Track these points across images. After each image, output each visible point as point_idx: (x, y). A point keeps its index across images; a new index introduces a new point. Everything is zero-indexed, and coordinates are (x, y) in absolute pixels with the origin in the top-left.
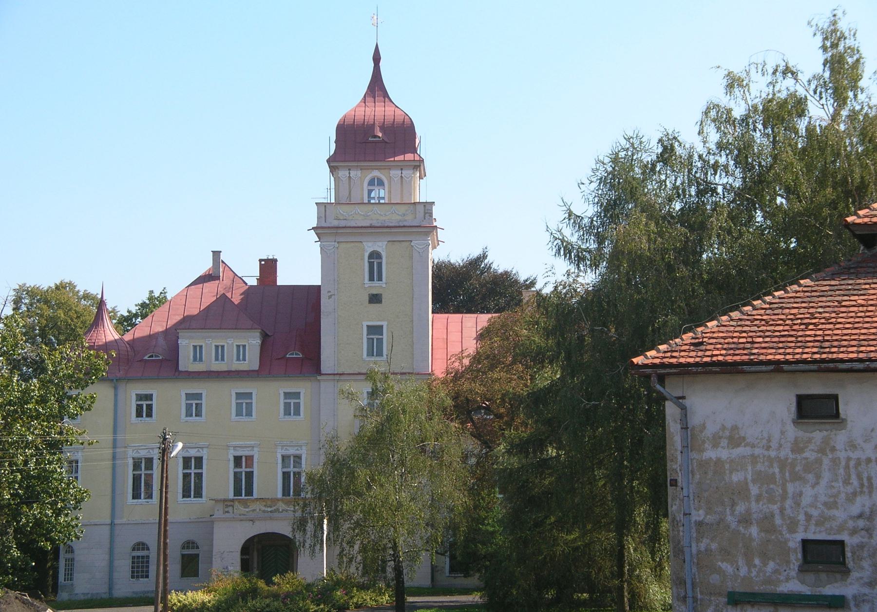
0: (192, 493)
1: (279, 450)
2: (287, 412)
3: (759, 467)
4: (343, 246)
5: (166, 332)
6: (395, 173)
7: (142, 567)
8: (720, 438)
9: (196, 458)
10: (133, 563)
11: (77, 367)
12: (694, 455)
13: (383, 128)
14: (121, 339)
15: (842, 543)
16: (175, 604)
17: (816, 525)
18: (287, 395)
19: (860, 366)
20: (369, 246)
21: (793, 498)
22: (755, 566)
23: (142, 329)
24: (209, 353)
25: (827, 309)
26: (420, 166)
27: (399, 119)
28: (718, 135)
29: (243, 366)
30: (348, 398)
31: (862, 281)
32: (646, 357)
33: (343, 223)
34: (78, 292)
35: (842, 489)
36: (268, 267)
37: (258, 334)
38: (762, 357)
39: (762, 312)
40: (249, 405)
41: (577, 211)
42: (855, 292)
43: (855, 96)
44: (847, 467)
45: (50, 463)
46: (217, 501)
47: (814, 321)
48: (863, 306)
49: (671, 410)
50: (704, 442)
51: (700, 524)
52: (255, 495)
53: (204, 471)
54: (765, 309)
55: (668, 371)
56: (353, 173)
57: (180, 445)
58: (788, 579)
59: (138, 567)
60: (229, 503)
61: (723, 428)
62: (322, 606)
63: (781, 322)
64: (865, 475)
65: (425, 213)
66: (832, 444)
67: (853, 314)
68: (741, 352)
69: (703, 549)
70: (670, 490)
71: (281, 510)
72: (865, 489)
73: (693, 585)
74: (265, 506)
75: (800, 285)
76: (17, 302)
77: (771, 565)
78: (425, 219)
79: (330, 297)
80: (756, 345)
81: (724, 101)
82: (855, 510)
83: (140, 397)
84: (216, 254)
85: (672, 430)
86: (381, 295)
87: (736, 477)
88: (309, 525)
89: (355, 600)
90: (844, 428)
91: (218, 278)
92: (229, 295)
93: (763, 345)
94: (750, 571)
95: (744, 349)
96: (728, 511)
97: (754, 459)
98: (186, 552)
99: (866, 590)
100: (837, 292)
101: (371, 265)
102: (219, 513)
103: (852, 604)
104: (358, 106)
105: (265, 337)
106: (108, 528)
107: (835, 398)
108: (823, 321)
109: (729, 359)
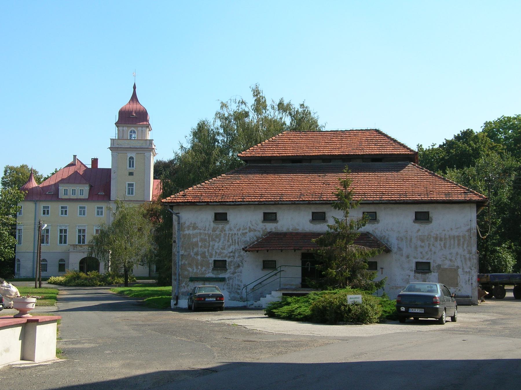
0: (82, 242)
1: (77, 227)
2: (98, 214)
3: (202, 236)
5: (55, 184)
6: (140, 129)
8: (190, 227)
9: (64, 230)
11: (14, 196)
12: (181, 232)
13: (136, 112)
14: (38, 186)
15: (226, 261)
16: (52, 281)
17: (218, 255)
18: (98, 208)
19: (233, 203)
20: (129, 155)
21: (212, 247)
22: (199, 269)
23: (46, 183)
24: (70, 192)
25: (228, 184)
26: (149, 126)
27: (142, 109)
28: (221, 123)
29: (82, 197)
30: (109, 210)
31: (241, 175)
32: (166, 199)
33: (120, 146)
34: (29, 168)
35: (227, 244)
36: (95, 161)
38: (203, 200)
39: (208, 185)
40: (84, 211)
41: (184, 146)
42: (237, 179)
43: (266, 112)
44: (229, 236)
45: (2, 230)
46: (71, 245)
47: (222, 188)
48: (239, 183)
49: (174, 217)
50: (185, 228)
51: (182, 255)
52: (86, 244)
53: (49, 234)
54: (209, 184)
55: (173, 204)
57: (46, 225)
58: (209, 273)
60: (75, 246)
61: (191, 224)
62: (102, 283)
63: (212, 188)
64: (234, 239)
65: (150, 143)
66: (225, 229)
67: (235, 186)
68: (198, 198)
69: (183, 263)
70: (173, 244)
72: (233, 244)
73: (179, 275)
75: (221, 176)
76: (6, 172)
77: (204, 268)
79: (115, 173)
80: (202, 196)
81: (221, 111)
82: (230, 250)
83: (44, 207)
84: (75, 156)
85: (175, 224)
87: (195, 240)
88: (93, 254)
89: (116, 281)
90: (228, 224)
91: (75, 165)
92: (79, 172)
93: (205, 196)
94: (197, 271)
95: (198, 197)
96: (191, 251)
97: (200, 234)
99: (231, 275)
100: (232, 179)
101: (130, 162)
102: (71, 250)
103: (227, 280)
104: (127, 104)
105: (91, 187)
106: (32, 253)
107: (226, 214)
108: (225, 188)
109: (193, 201)
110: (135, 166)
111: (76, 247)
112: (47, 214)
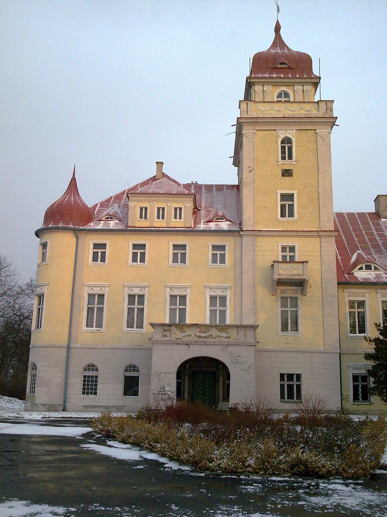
1: (168, 290)
4: (260, 133)
7: (92, 385)
10: (84, 381)
24: (152, 213)
37: (192, 199)
59: (88, 385)
71: (214, 336)
74: (199, 332)
78: (327, 113)
79: (250, 171)
83: (96, 246)
86: (292, 170)
98: (129, 374)
101: (283, 148)
102: (158, 337)
111: (170, 331)
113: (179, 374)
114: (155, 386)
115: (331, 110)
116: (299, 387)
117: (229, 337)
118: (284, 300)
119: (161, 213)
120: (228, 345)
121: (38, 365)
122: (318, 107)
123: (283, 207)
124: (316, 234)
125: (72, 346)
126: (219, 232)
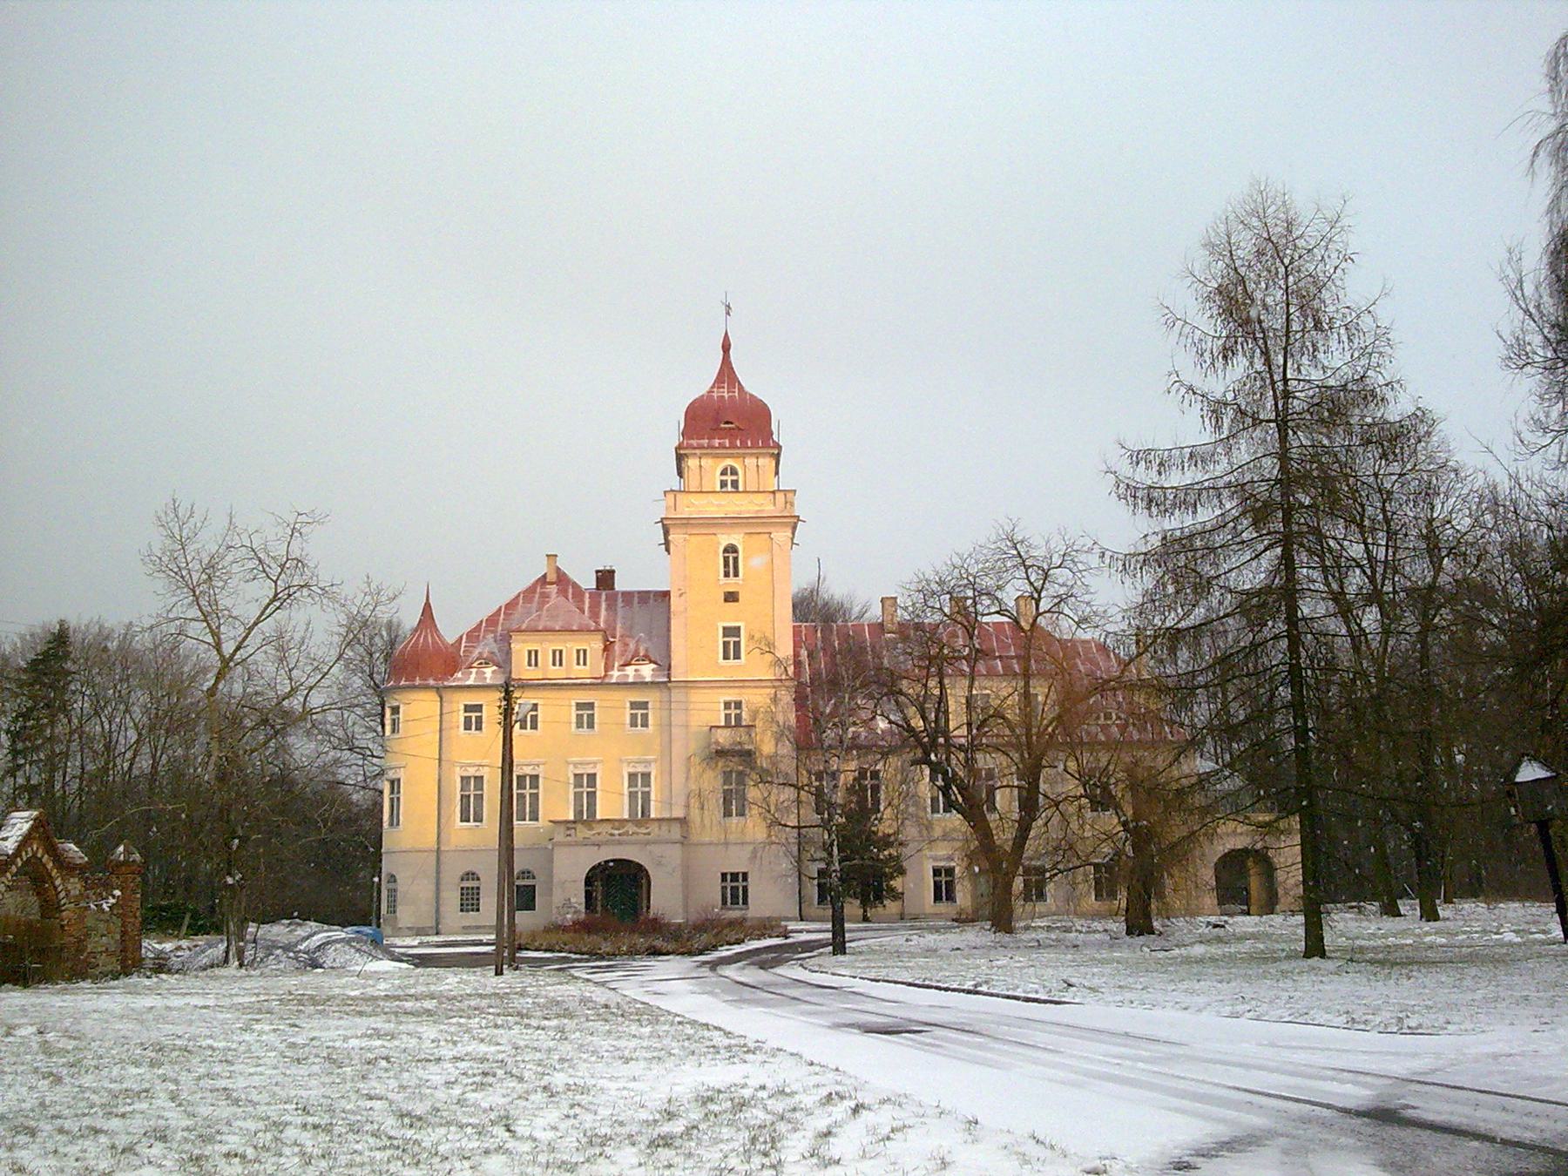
4: (693, 539)
7: (467, 899)
10: (462, 894)
24: (546, 658)
37: (600, 637)
56: (704, 462)
79: (681, 595)
83: (468, 708)
98: (466, 884)
102: (560, 837)
110: (744, 574)
111: (575, 829)
112: (476, 729)
113: (589, 881)
114: (558, 898)
115: (792, 504)
116: (745, 889)
117: (649, 834)
118: (727, 776)
119: (558, 658)
120: (648, 843)
121: (397, 877)
122: (775, 498)
123: (726, 644)
124: (769, 684)
125: (442, 848)
126: (639, 685)
